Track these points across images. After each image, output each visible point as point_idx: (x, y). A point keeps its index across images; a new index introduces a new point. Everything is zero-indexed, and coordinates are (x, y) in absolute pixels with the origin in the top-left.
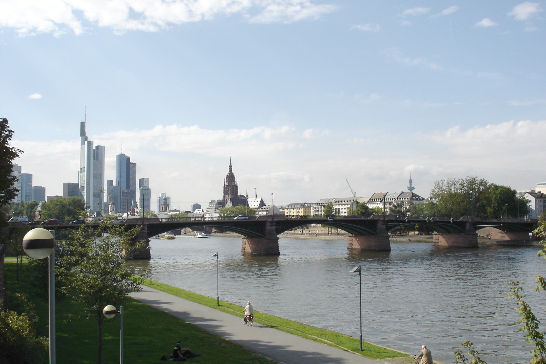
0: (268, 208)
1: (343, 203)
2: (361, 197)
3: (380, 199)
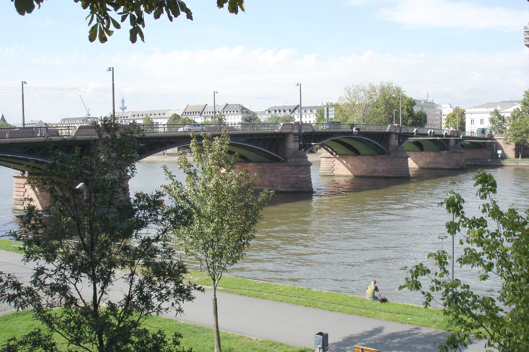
0: (32, 124)
1: (161, 116)
2: (169, 110)
3: (199, 112)
